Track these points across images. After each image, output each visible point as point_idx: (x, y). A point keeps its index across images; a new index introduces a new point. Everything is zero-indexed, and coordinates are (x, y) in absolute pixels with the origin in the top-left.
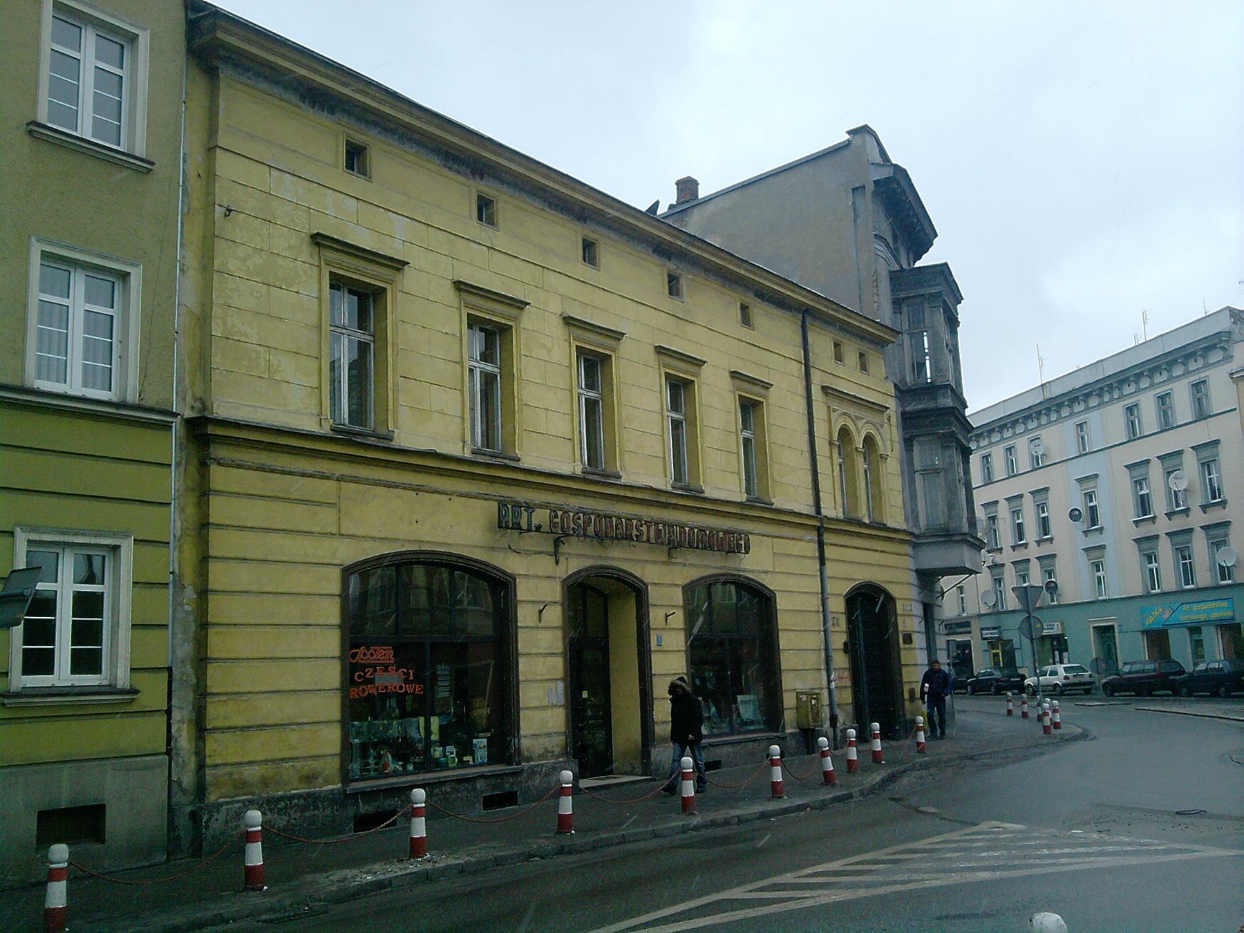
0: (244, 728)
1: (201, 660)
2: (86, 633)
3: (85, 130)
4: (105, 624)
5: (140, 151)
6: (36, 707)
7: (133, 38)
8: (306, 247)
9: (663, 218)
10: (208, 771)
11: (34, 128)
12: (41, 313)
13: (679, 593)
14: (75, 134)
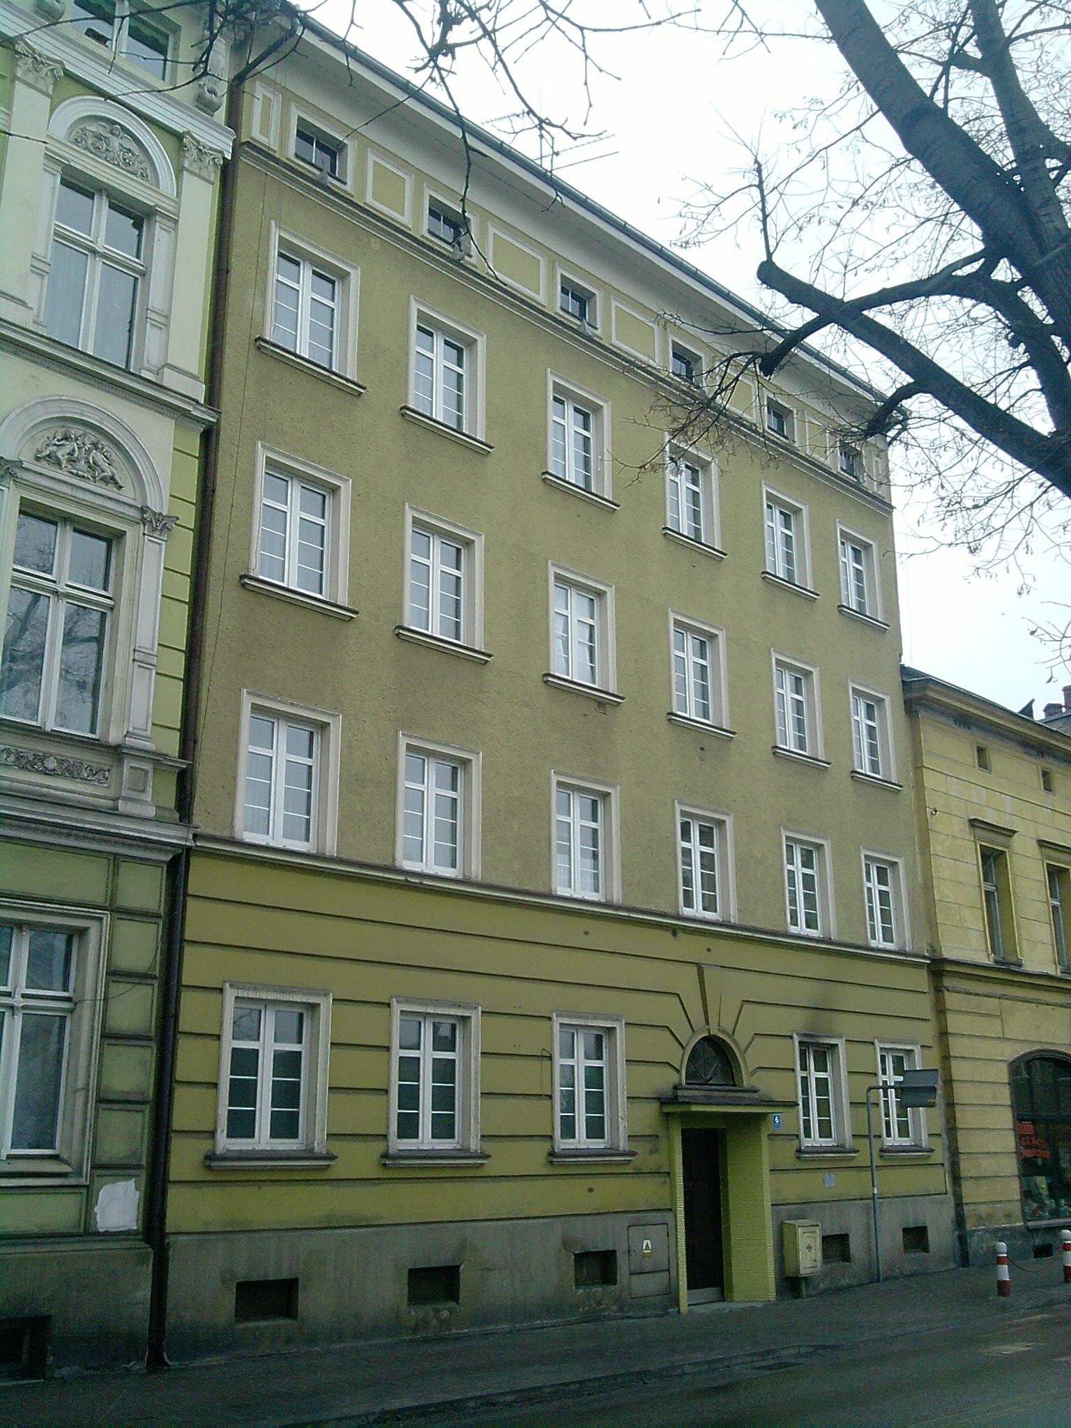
0: (977, 1178)
1: (950, 1129)
2: (287, 1094)
3: (291, 581)
4: (457, 1090)
5: (343, 599)
6: (897, 1158)
7: (334, 490)
8: (967, 828)
9: (1046, 723)
10: (965, 1208)
11: (401, 631)
12: (683, 853)
13: (1004, 1069)
14: (566, 677)
